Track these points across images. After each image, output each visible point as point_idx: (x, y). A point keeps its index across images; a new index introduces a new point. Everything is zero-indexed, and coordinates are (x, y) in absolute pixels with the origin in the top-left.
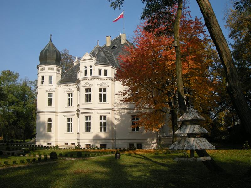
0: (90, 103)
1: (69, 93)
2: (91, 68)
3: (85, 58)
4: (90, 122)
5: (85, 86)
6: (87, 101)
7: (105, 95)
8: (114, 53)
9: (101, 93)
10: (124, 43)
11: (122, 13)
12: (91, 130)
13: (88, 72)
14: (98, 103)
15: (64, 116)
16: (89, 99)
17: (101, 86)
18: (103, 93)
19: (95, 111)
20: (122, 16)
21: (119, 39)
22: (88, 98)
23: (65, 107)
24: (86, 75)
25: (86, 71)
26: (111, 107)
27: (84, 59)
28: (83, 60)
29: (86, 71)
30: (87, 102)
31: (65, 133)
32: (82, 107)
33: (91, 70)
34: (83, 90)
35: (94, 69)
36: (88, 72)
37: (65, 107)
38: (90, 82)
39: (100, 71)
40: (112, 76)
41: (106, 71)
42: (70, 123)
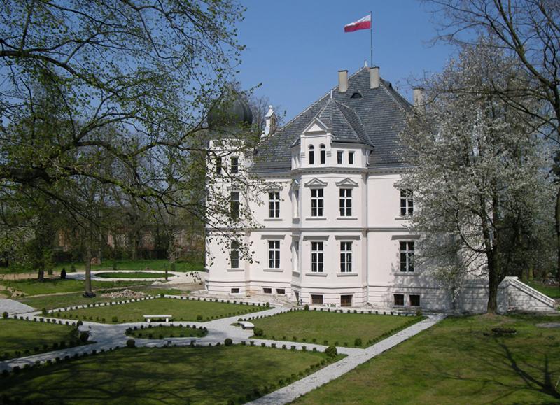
0: (320, 217)
1: (342, 188)
2: (323, 150)
3: (312, 130)
4: (279, 252)
5: (311, 186)
6: (314, 213)
7: (349, 203)
8: (358, 110)
9: (314, 198)
10: (377, 86)
11: (368, 18)
12: (324, 268)
13: (317, 157)
14: (338, 219)
15: (337, 238)
16: (347, 209)
17: (343, 185)
18: (346, 198)
19: (332, 235)
20: (365, 26)
21: (365, 75)
22: (318, 208)
23: (396, 219)
24: (312, 161)
25: (312, 154)
26: (360, 227)
27: (310, 131)
28: (308, 134)
29: (312, 154)
30: (316, 215)
31: (338, 276)
32: (304, 224)
33: (323, 154)
34: (306, 194)
35: (329, 153)
36: (317, 157)
37: (396, 219)
38: (322, 178)
39: (340, 154)
40: (363, 164)
41: (351, 155)
42: (346, 252)
